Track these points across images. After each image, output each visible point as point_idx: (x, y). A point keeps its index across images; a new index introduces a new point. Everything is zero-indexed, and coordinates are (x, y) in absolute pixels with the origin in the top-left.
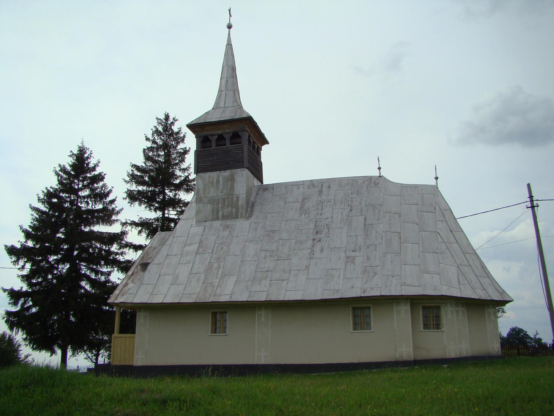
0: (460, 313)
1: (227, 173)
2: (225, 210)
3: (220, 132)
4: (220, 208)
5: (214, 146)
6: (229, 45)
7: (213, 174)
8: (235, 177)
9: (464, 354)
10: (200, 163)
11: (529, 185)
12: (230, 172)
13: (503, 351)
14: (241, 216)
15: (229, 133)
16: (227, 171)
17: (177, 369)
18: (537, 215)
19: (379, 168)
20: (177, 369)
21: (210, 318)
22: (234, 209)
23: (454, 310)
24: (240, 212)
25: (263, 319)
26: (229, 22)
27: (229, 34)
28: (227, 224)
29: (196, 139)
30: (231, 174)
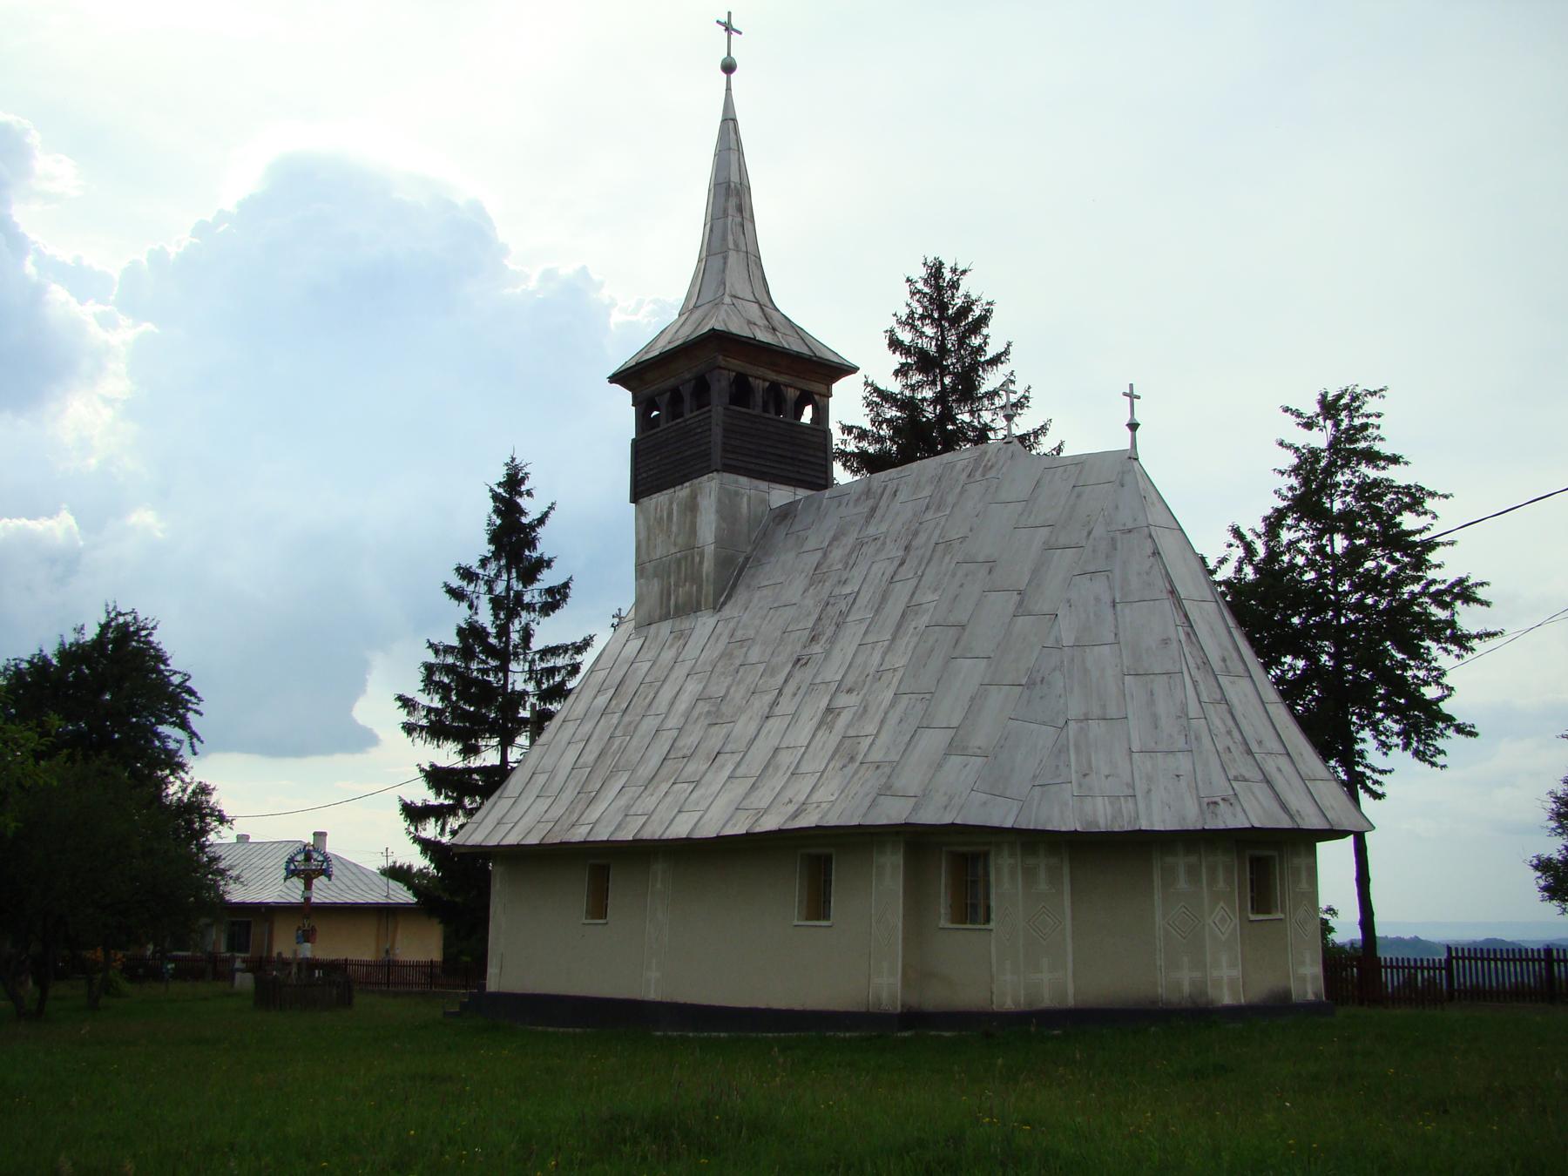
0: (1042, 874)
1: (683, 492)
2: (681, 589)
3: (671, 382)
4: (673, 587)
6: (729, 122)
7: (662, 497)
8: (699, 498)
9: (1047, 1000)
10: (641, 471)
11: (1281, 444)
12: (690, 486)
14: (705, 605)
15: (690, 380)
16: (685, 485)
17: (116, 1066)
20: (116, 1066)
21: (587, 879)
22: (695, 587)
23: (1019, 868)
24: (704, 592)
26: (726, 55)
27: (728, 89)
28: (683, 627)
29: (634, 408)
30: (692, 491)
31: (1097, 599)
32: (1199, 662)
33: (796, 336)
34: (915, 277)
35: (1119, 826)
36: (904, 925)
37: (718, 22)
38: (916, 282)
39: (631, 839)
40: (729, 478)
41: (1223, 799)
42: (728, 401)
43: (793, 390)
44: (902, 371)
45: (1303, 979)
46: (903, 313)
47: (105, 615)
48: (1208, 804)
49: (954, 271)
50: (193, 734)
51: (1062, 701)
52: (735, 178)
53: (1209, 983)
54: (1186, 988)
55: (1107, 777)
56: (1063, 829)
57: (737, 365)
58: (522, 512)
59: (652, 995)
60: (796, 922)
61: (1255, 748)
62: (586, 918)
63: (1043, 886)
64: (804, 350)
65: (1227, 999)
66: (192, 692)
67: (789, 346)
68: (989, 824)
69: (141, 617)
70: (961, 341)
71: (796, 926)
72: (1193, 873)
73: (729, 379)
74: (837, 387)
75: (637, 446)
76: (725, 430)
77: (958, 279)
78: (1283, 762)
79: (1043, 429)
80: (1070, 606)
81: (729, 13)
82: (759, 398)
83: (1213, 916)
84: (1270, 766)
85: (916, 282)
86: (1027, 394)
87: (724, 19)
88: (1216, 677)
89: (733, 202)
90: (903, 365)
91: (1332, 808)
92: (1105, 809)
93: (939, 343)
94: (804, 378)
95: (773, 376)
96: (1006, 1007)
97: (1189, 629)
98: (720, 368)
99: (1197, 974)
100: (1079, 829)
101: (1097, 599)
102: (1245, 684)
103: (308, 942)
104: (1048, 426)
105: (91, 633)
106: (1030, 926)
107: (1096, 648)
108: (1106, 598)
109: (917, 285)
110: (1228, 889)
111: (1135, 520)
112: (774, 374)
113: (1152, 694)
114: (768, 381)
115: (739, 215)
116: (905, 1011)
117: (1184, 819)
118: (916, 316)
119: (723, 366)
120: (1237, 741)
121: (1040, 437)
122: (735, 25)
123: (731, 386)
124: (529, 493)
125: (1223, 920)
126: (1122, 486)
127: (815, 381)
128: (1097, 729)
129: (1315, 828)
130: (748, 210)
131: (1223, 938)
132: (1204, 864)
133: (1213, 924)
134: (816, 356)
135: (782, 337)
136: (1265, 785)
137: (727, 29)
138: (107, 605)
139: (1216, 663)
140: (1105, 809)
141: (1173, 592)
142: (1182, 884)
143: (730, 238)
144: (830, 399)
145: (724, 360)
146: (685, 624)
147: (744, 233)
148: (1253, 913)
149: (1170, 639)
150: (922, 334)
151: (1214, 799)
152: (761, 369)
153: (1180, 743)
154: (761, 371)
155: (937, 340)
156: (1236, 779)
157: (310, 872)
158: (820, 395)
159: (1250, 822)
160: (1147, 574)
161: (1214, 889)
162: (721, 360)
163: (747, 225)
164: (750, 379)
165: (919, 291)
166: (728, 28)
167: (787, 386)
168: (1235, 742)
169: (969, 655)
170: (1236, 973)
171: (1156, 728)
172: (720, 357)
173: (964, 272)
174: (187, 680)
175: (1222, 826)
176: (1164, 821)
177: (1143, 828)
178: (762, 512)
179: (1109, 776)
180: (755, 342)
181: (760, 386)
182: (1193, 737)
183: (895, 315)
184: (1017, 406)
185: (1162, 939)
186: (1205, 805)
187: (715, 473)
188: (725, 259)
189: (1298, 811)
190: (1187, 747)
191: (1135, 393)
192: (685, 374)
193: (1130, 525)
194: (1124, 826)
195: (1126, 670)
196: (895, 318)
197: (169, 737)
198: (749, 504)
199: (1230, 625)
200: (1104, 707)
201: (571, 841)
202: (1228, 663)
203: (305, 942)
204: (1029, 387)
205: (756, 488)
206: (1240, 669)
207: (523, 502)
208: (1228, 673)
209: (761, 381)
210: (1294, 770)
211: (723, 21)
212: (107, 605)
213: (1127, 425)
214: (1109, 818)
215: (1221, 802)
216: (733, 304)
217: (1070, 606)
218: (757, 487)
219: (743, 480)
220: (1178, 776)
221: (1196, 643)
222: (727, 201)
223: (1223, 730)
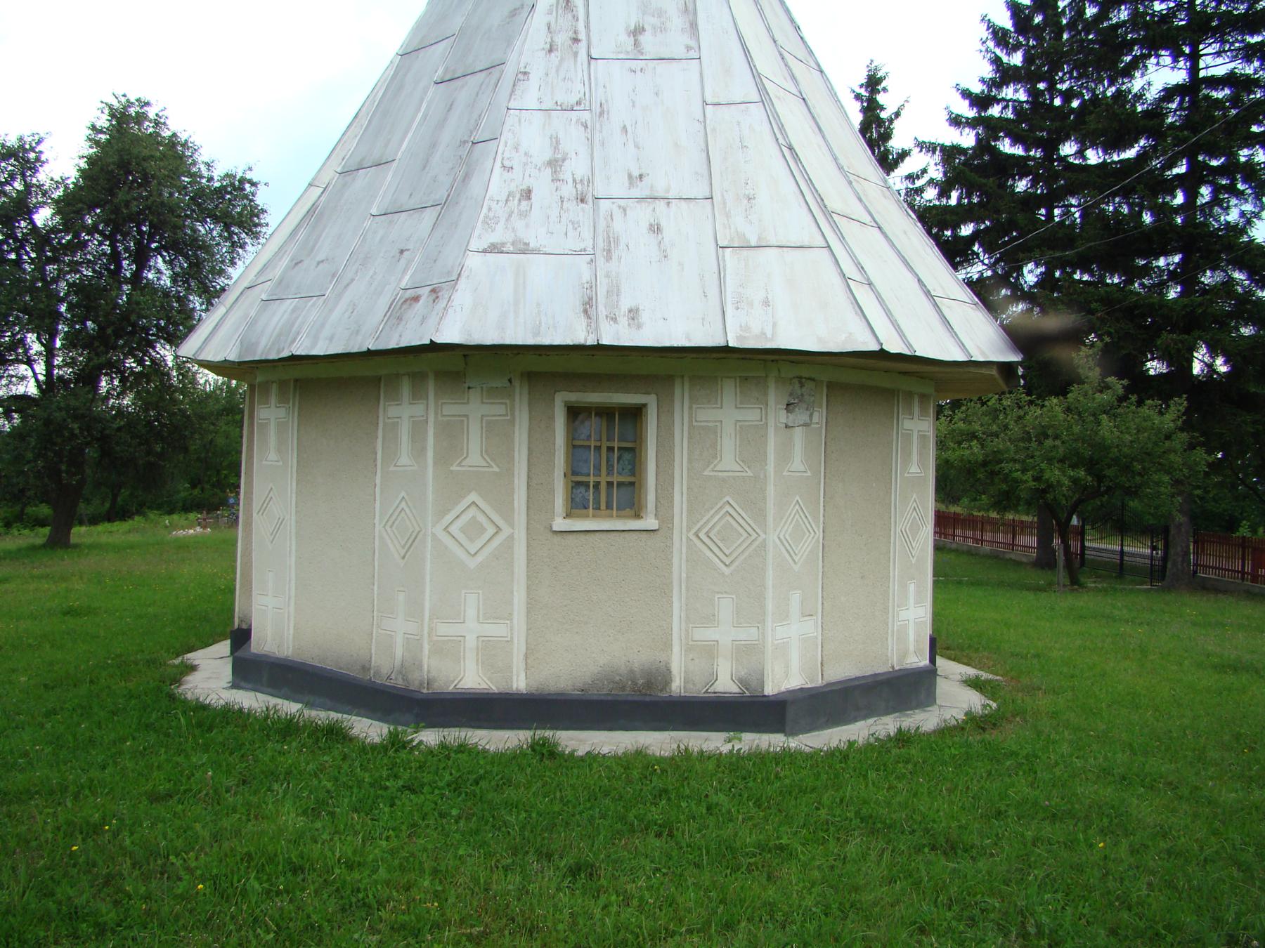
25: (474, 456)
32: (562, 39)
45: (710, 651)
53: (426, 647)
58: (882, 108)
63: (474, 456)
72: (752, 440)
99: (747, 634)
110: (496, 469)
124: (885, 90)
131: (472, 563)
133: (777, 541)
142: (728, 461)
161: (454, 468)
170: (810, 628)
207: (881, 98)
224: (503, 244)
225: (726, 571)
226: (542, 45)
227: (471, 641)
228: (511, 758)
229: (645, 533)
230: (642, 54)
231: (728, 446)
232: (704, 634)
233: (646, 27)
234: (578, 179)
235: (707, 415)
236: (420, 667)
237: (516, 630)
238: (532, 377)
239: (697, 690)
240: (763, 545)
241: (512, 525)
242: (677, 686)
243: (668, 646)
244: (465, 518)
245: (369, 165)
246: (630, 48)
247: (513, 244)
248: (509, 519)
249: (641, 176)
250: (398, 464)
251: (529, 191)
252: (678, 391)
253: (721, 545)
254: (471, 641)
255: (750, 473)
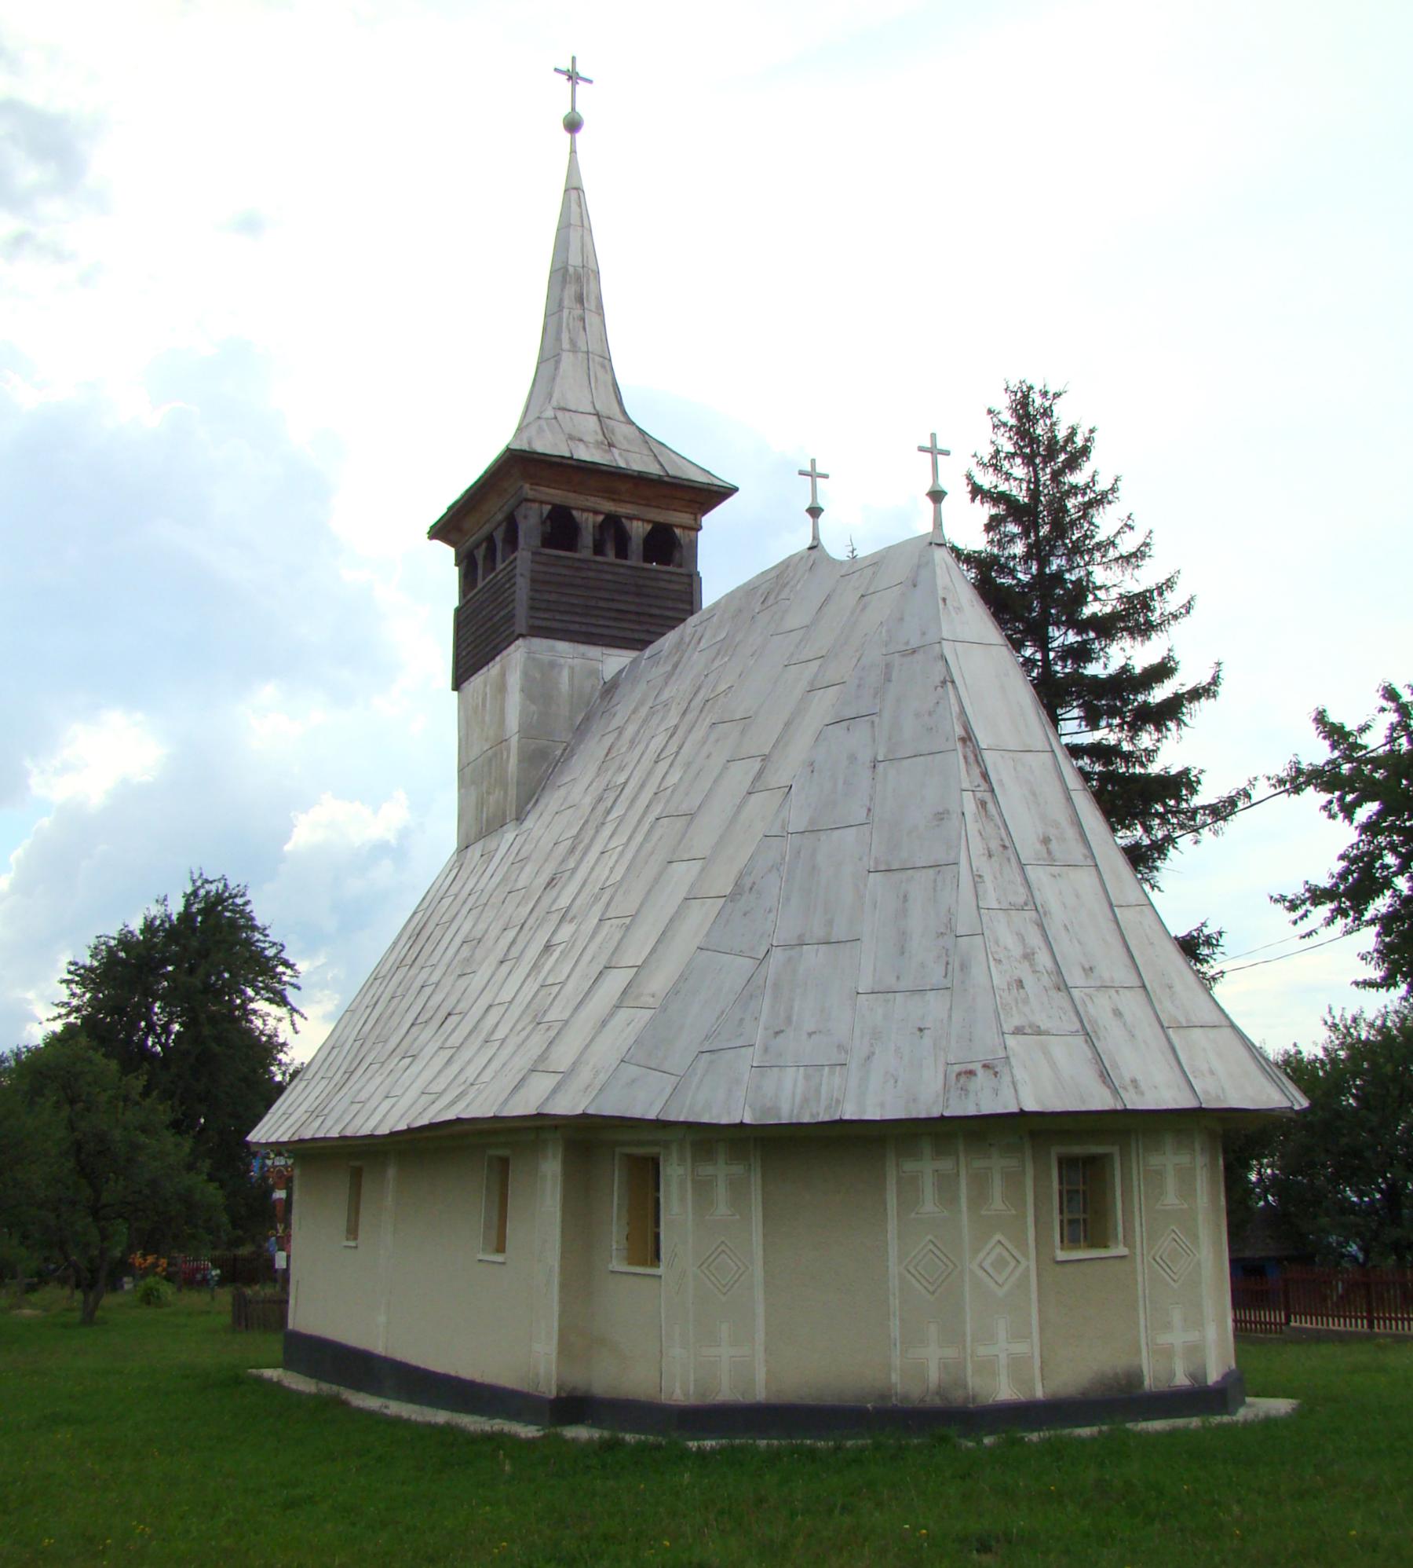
0: (721, 1191)
5: (585, 552)
6: (574, 190)
9: (726, 1392)
13: (1239, 1325)
18: (452, 852)
19: (815, 512)
23: (689, 1178)
25: (997, 1203)
26: (570, 110)
27: (573, 151)
31: (853, 758)
32: (994, 845)
33: (646, 452)
34: (996, 408)
35: (812, 1115)
36: (563, 1269)
37: (556, 70)
38: (998, 413)
39: (337, 1136)
40: (538, 644)
41: (985, 1066)
42: (540, 544)
43: (640, 523)
44: (993, 524)
45: (1168, 1352)
46: (986, 453)
47: (191, 883)
48: (959, 1075)
49: (1044, 394)
50: (293, 1010)
51: (772, 916)
52: (574, 260)
54: (934, 1376)
55: (810, 1034)
56: (724, 1120)
57: (557, 495)
59: (379, 1348)
60: (481, 1256)
61: (1075, 977)
62: (347, 1240)
63: (997, 1203)
64: (653, 469)
65: (1005, 1391)
66: (286, 964)
67: (627, 463)
68: (628, 1114)
69: (232, 884)
70: (1056, 476)
71: (480, 1261)
72: (946, 1187)
73: (542, 513)
74: (710, 520)
75: (458, 612)
76: (533, 581)
77: (1051, 405)
78: (1132, 1004)
79: (1169, 584)
80: (812, 772)
81: (574, 59)
82: (587, 538)
83: (981, 1255)
84: (1099, 1008)
85: (998, 413)
86: (1148, 540)
87: (567, 65)
88: (1022, 867)
89: (571, 291)
90: (993, 518)
91: (1212, 1073)
92: (795, 1085)
93: (1032, 486)
94: (658, 507)
95: (609, 506)
96: (675, 1397)
97: (987, 796)
98: (527, 500)
99: (950, 1352)
100: (747, 1120)
101: (853, 758)
102: (1085, 879)
103: (283, 1250)
104: (1176, 579)
105: (176, 907)
106: (702, 1272)
107: (837, 833)
108: (865, 757)
109: (1000, 417)
110: (1014, 1212)
111: (924, 634)
112: (611, 504)
113: (905, 898)
114: (601, 513)
115: (578, 306)
116: (563, 1395)
117: (914, 1100)
118: (1002, 455)
119: (529, 497)
120: (1040, 968)
121: (1165, 593)
122: (581, 70)
123: (543, 523)
125: (1000, 1264)
126: (915, 586)
127: (675, 510)
128: (812, 957)
129: (1164, 1107)
130: (593, 297)
131: (1001, 1292)
132: (963, 1172)
134: (668, 476)
135: (620, 455)
136: (1080, 1040)
137: (570, 78)
138: (192, 873)
139: (1027, 843)
140: (795, 1085)
141: (968, 738)
143: (565, 337)
144: (700, 534)
145: (531, 489)
146: (491, 843)
147: (584, 329)
148: (1062, 1249)
149: (948, 812)
150: (1008, 476)
151: (971, 1067)
152: (593, 499)
153: (936, 975)
154: (593, 502)
155: (1029, 482)
156: (1018, 1031)
157: (282, 1168)
158: (684, 528)
159: (1018, 1104)
160: (930, 714)
161: (983, 1212)
162: (528, 490)
163: (591, 319)
164: (575, 513)
165: (1005, 425)
166: (573, 77)
167: (631, 518)
168: (1035, 972)
169: (686, 857)
171: (903, 953)
172: (527, 486)
173: (1057, 395)
174: (282, 951)
175: (971, 1111)
176: (882, 1105)
177: (847, 1117)
178: (593, 686)
179: (815, 1033)
180: (574, 463)
181: (588, 522)
182: (957, 965)
183: (975, 456)
184: (1137, 557)
185: (897, 1294)
186: (954, 1075)
187: (521, 639)
188: (558, 363)
189: (1134, 1081)
190: (947, 983)
191: (939, 447)
192: (495, 511)
193: (914, 643)
194: (818, 1114)
195: (872, 863)
196: (976, 460)
197: (269, 1015)
198: (571, 679)
199: (1071, 786)
200: (830, 923)
201: (646, 1117)
202: (1054, 845)
203: (279, 1250)
204: (1151, 532)
205: (583, 656)
206: (1077, 852)
208: (1050, 860)
209: (591, 515)
210: (1151, 1013)
211: (564, 69)
212: (192, 873)
213: (927, 495)
214: (798, 1099)
215: (980, 1072)
216: (556, 418)
217: (812, 772)
218: (583, 655)
219: (562, 646)
220: (921, 1030)
221: (997, 817)
222: (562, 290)
223: (1017, 951)
224: (1023, 1027)
225: (1175, 1286)
226: (982, 851)
227: (1003, 1359)
228: (1093, 1439)
229: (1099, 1261)
230: (1054, 861)
231: (1171, 1183)
232: (1164, 1339)
233: (1051, 837)
234: (1049, 971)
235: (1155, 1160)
236: (965, 1386)
237: (1030, 1348)
238: (1034, 1135)
239: (1162, 1386)
240: (1199, 1264)
241: (1028, 1260)
242: (1148, 1383)
243: (1139, 1352)
244: (993, 1256)
245: (815, 941)
246: (1045, 855)
247: (1030, 1027)
248: (1026, 1255)
249: (1091, 969)
250: (1165, 1202)
251: (1021, 981)
252: (1133, 1145)
253: (1170, 1264)
254: (1003, 1356)
255: (1186, 1206)
